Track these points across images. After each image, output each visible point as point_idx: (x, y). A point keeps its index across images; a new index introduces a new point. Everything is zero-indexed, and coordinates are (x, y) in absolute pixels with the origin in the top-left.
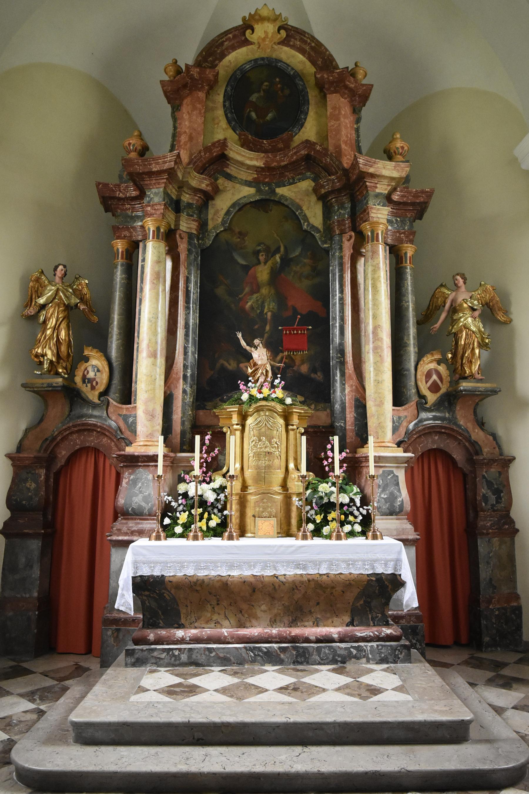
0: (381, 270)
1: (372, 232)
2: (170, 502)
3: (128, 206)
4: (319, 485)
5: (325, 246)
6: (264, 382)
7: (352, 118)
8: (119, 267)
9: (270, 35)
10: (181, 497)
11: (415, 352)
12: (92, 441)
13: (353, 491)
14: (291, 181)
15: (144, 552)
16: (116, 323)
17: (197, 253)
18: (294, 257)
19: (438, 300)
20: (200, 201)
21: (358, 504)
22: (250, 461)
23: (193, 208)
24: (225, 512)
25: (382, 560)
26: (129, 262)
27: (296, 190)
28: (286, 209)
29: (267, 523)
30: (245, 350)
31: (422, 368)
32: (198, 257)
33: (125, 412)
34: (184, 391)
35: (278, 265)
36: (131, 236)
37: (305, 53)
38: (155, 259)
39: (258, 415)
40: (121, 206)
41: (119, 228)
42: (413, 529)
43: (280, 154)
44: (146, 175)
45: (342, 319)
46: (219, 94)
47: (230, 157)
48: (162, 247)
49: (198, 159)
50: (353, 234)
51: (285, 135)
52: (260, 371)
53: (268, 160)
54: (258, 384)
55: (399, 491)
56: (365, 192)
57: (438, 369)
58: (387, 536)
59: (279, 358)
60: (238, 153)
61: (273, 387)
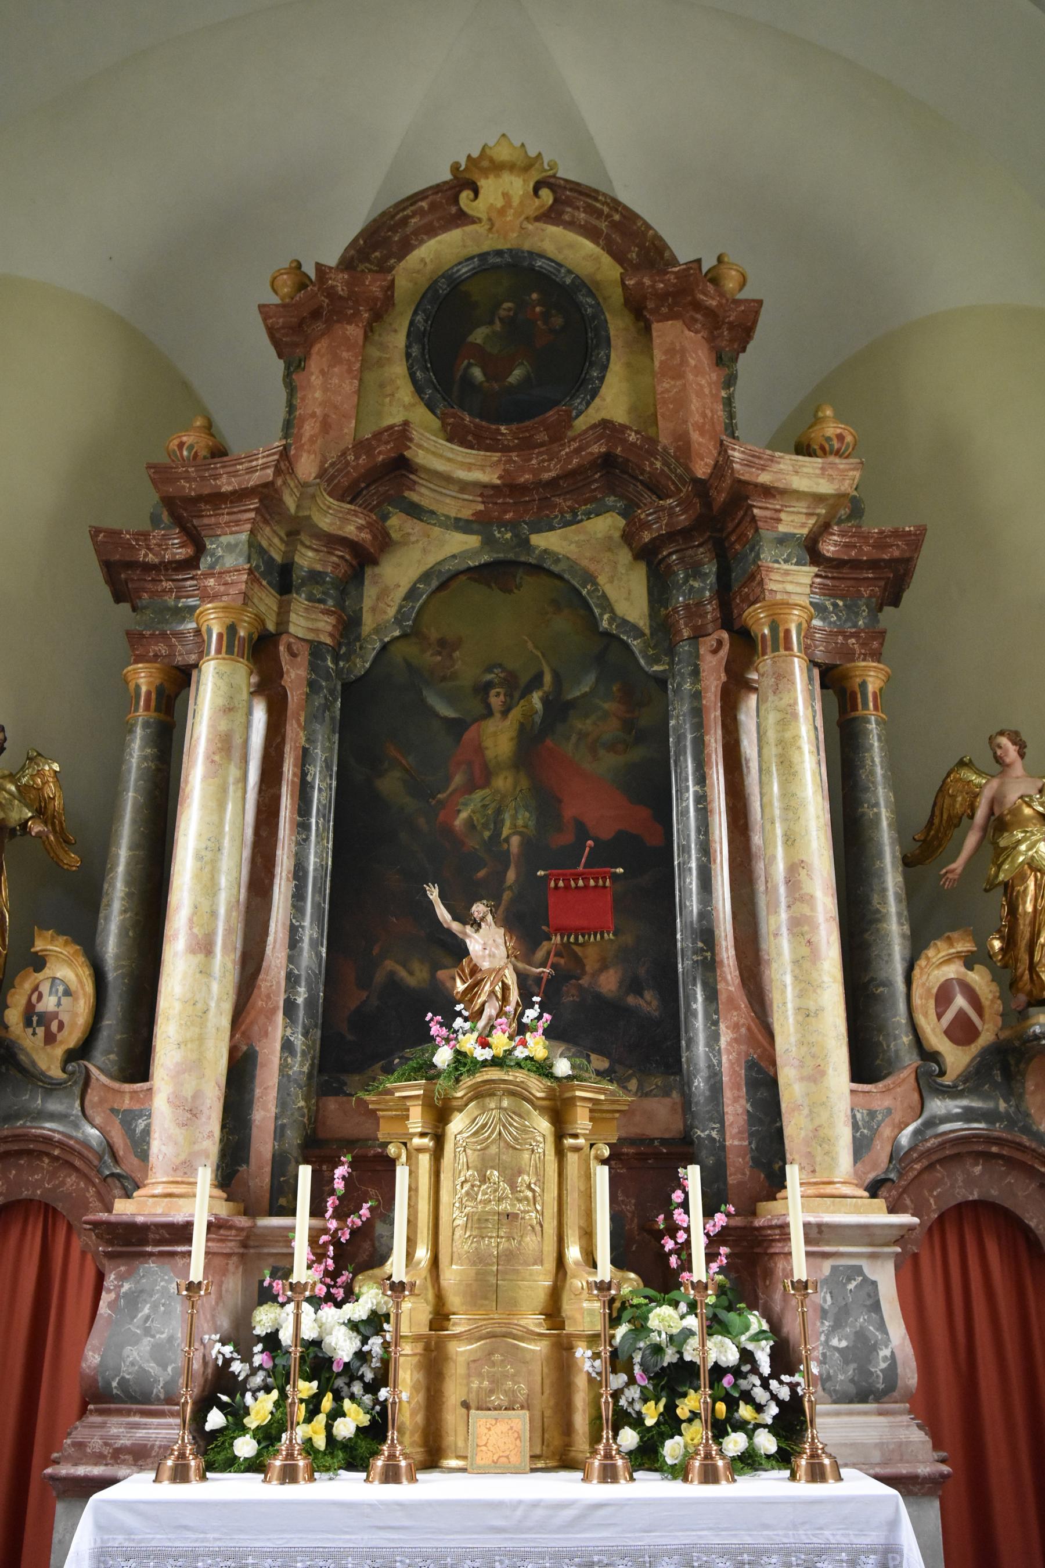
0: (802, 720)
1: (774, 627)
2: (227, 1362)
3: (169, 585)
4: (650, 1311)
5: (656, 668)
6: (498, 1016)
7: (714, 376)
8: (139, 731)
9: (516, 202)
10: (259, 1347)
11: (903, 936)
12: (37, 1185)
13: (747, 1328)
14: (568, 516)
15: (130, 1521)
16: (121, 869)
17: (332, 692)
18: (578, 698)
19: (955, 801)
20: (343, 568)
21: (766, 1369)
22: (458, 1240)
23: (324, 582)
24: (383, 1393)
25: (842, 1550)
26: (162, 717)
27: (582, 537)
28: (557, 582)
29: (502, 1427)
30: (449, 932)
31: (925, 977)
32: (335, 700)
33: (127, 1102)
34: (287, 1046)
35: (538, 719)
36: (171, 655)
37: (599, 238)
38: (220, 701)
39: (477, 1106)
40: (150, 586)
41: (142, 636)
42: (930, 1445)
43: (540, 454)
44: (206, 503)
45: (706, 849)
46: (395, 331)
47: (417, 464)
48: (242, 675)
49: (339, 471)
50: (725, 635)
51: (551, 415)
52: (487, 988)
53: (511, 467)
54: (481, 1024)
55: (882, 1326)
56: (750, 534)
57: (968, 980)
58: (854, 1466)
59: (540, 954)
60: (435, 452)
61: (522, 1029)
